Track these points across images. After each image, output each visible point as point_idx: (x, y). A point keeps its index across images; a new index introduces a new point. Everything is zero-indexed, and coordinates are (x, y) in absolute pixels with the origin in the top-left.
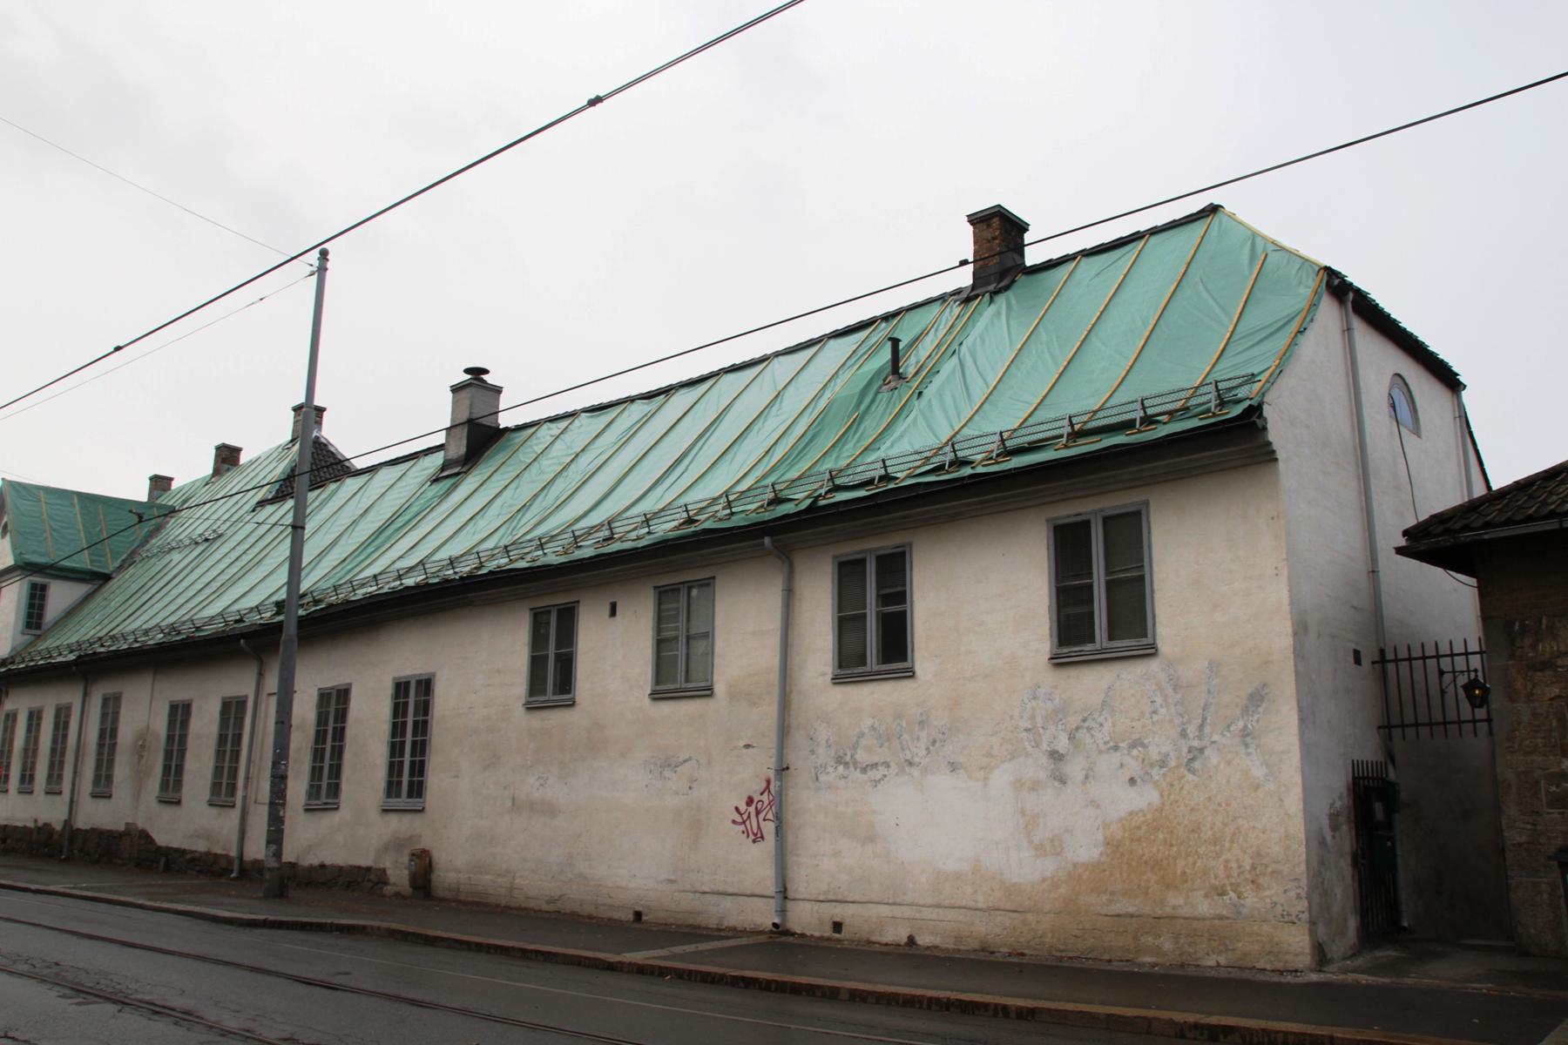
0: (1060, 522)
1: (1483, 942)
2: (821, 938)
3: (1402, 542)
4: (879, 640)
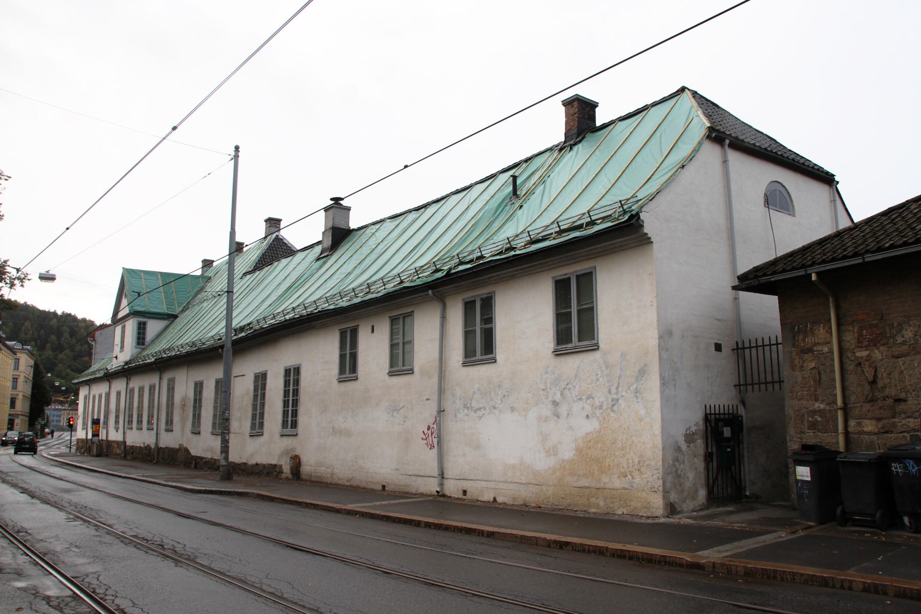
0: (579, 273)
1: (782, 503)
2: (458, 499)
3: (737, 283)
4: (481, 345)
